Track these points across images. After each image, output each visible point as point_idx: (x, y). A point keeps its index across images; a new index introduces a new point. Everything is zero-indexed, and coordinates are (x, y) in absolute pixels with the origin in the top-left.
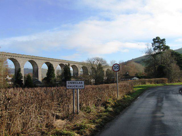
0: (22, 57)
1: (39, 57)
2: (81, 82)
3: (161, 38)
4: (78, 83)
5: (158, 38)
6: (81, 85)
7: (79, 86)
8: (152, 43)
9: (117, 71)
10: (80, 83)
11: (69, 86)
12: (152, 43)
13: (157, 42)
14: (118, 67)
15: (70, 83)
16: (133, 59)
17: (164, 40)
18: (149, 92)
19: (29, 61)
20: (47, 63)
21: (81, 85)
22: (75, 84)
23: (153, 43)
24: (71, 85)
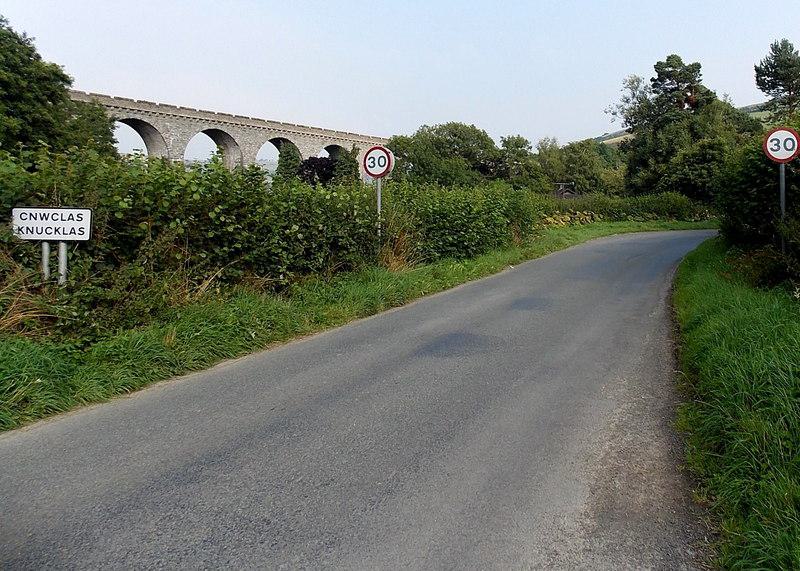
0: (242, 122)
1: (151, 104)
2: (75, 212)
3: (687, 62)
4: (66, 217)
5: (674, 60)
6: (77, 225)
7: (67, 231)
8: (652, 80)
9: (377, 176)
10: (71, 217)
11: (24, 230)
12: (652, 80)
13: (669, 75)
14: (382, 162)
15: (28, 216)
16: (588, 142)
17: (697, 67)
18: (640, 230)
19: (208, 132)
20: (276, 142)
21: (77, 225)
22: (50, 222)
23: (656, 77)
24: (31, 223)
